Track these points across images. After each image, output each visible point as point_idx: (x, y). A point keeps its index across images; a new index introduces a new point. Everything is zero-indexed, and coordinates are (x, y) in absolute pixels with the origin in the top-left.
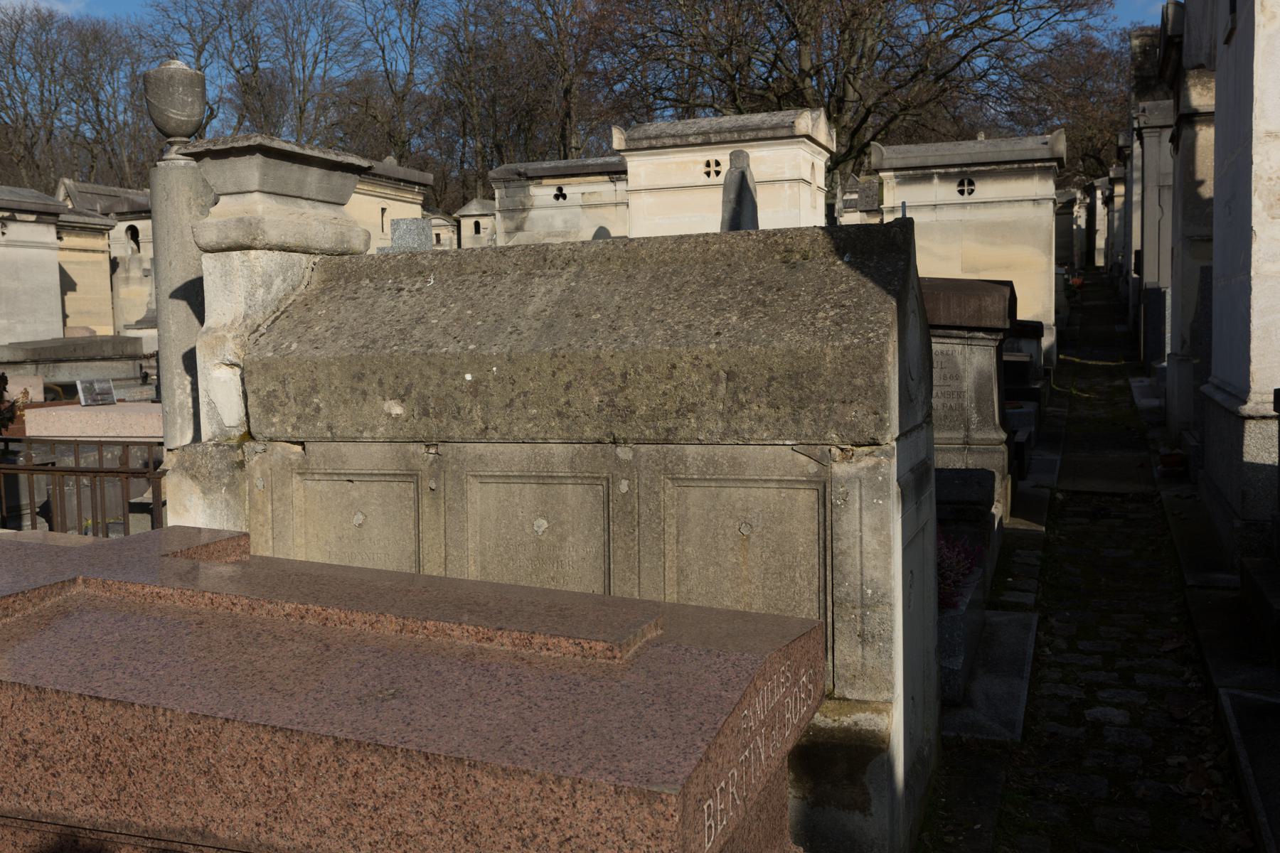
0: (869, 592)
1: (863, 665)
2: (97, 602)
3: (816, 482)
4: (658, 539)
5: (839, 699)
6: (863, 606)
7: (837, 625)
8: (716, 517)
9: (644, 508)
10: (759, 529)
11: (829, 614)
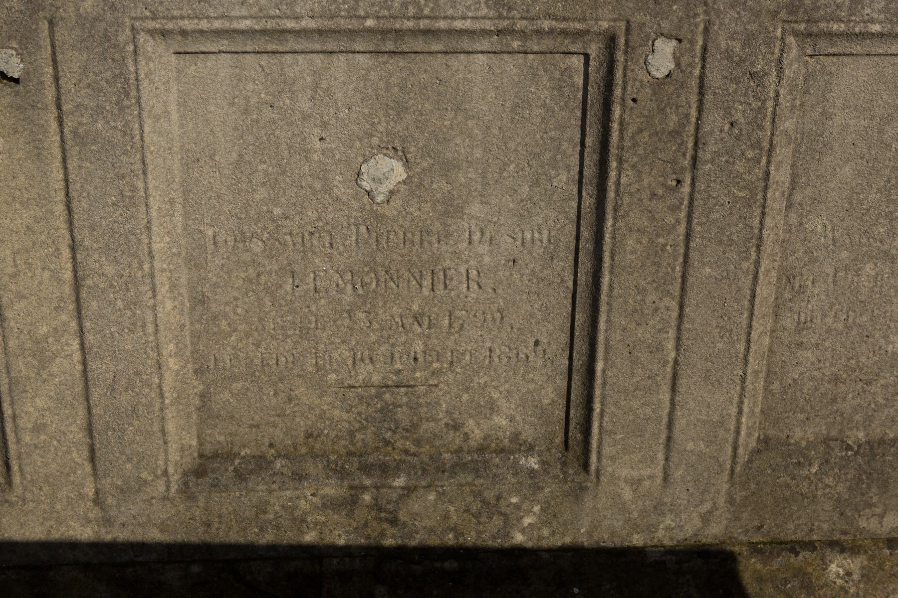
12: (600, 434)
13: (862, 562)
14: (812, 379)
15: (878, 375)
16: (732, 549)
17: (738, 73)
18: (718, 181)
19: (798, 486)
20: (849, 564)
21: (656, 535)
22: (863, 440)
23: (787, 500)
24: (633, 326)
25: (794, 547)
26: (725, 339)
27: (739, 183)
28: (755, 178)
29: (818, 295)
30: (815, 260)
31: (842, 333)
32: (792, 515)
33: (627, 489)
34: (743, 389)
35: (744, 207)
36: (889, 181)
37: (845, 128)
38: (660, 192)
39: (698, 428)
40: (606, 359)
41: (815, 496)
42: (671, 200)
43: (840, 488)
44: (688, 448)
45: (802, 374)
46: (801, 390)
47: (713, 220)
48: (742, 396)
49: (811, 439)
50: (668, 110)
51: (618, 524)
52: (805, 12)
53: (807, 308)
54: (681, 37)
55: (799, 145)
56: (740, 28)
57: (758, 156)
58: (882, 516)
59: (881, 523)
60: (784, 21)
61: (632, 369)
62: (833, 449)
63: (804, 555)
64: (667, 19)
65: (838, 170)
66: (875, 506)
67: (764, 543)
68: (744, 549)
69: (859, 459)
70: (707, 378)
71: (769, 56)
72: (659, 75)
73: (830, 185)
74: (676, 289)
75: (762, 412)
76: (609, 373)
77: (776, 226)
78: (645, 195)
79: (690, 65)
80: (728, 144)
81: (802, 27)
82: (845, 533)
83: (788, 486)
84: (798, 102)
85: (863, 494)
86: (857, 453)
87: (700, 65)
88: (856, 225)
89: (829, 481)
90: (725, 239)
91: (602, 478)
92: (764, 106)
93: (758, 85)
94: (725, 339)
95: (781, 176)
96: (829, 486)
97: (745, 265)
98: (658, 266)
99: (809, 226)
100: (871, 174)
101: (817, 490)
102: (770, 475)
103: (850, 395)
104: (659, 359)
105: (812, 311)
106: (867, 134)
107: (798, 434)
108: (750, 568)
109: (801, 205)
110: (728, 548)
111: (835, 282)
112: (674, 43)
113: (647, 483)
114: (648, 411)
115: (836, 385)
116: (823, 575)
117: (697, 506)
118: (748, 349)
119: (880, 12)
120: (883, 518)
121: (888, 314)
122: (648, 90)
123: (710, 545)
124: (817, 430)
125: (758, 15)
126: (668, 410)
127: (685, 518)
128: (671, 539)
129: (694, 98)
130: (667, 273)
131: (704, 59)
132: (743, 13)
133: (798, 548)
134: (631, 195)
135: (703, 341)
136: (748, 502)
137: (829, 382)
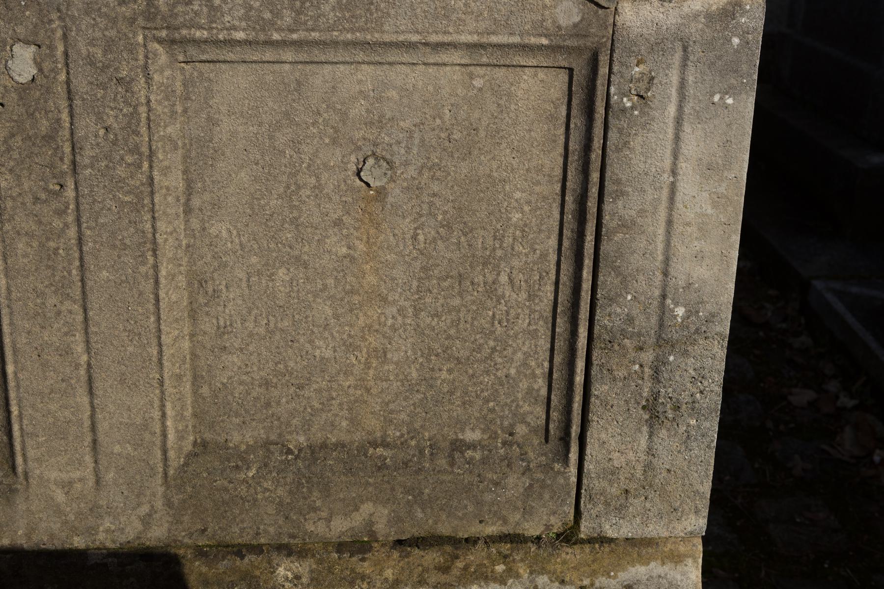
0: (680, 311)
1: (648, 467)
2: (697, 405)
3: (569, 50)
4: (136, 208)
5: (590, 541)
6: (662, 342)
7: (599, 389)
8: (295, 143)
9: (87, 125)
10: (412, 171)
11: (580, 365)
12: (22, 436)
13: (310, 566)
14: (241, 383)
15: (309, 379)
16: (177, 552)
17: (103, 78)
18: (101, 185)
19: (236, 489)
20: (297, 567)
21: (98, 537)
22: (305, 444)
23: (227, 503)
24: (37, 329)
25: (240, 550)
26: (135, 342)
27: (122, 187)
28: (138, 183)
29: (234, 299)
30: (225, 265)
31: (264, 338)
32: (235, 518)
33: (59, 491)
34: (163, 392)
35: (132, 211)
36: (288, 187)
37: (234, 134)
38: (43, 196)
39: (122, 431)
40: (16, 362)
41: (256, 500)
42: (55, 205)
43: (280, 492)
44: (115, 451)
45: (230, 378)
46: (232, 394)
47: (103, 225)
48: (162, 400)
49: (251, 443)
50: (37, 114)
51: (56, 527)
52: (164, 18)
53: (224, 312)
54: (39, 43)
55: (189, 151)
56: (98, 34)
57: (138, 161)
58: (329, 520)
59: (328, 527)
60: (144, 28)
61: (44, 372)
62: (273, 453)
63: (250, 558)
64: (21, 24)
65: (234, 175)
66: (319, 510)
67: (210, 546)
68: (189, 552)
69: (300, 463)
70: (122, 381)
71: (133, 62)
72: (21, 80)
73: (227, 190)
74: (77, 292)
75: (195, 415)
76: (20, 376)
77: (175, 230)
78: (28, 199)
79: (52, 70)
80: (105, 149)
81: (164, 33)
82: (293, 536)
83: (226, 490)
84: (179, 109)
85: (305, 498)
86: (297, 457)
87: (65, 71)
88: (261, 230)
89: (268, 484)
90: (118, 243)
91: (31, 480)
92: (136, 112)
93: (127, 91)
94: (135, 342)
95: (172, 181)
96: (268, 490)
97: (143, 269)
98: (53, 270)
99: (213, 231)
100: (268, 180)
101: (256, 493)
102: (206, 478)
103: (284, 400)
104: (71, 362)
105: (231, 316)
106: (258, 139)
107: (236, 438)
108: (195, 570)
109: (201, 210)
110: (173, 551)
111: (249, 287)
112: (33, 48)
113: (78, 486)
114: (67, 413)
115: (267, 389)
116: (272, 578)
117: (134, 509)
118: (160, 352)
119: (240, 19)
120: (330, 521)
121: (310, 319)
122: (13, 95)
123: (156, 547)
124: (256, 433)
125: (114, 21)
126: (89, 413)
127: (126, 519)
128: (114, 542)
129: (64, 104)
130: (64, 277)
131: (67, 65)
132: (99, 20)
133: (244, 551)
134: (13, 199)
135: (112, 344)
136: (186, 505)
137: (260, 386)
